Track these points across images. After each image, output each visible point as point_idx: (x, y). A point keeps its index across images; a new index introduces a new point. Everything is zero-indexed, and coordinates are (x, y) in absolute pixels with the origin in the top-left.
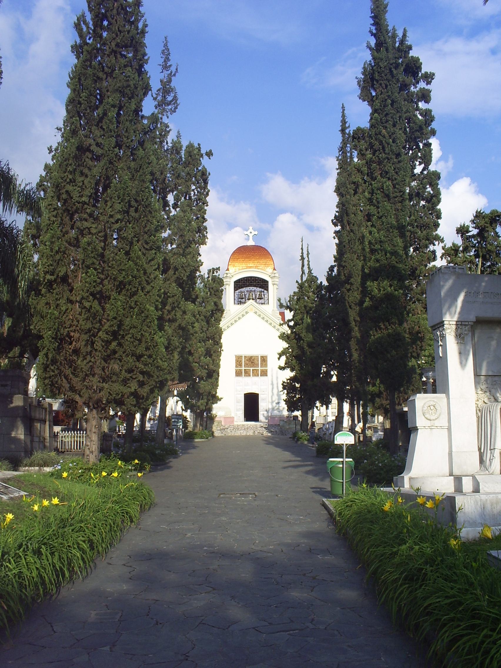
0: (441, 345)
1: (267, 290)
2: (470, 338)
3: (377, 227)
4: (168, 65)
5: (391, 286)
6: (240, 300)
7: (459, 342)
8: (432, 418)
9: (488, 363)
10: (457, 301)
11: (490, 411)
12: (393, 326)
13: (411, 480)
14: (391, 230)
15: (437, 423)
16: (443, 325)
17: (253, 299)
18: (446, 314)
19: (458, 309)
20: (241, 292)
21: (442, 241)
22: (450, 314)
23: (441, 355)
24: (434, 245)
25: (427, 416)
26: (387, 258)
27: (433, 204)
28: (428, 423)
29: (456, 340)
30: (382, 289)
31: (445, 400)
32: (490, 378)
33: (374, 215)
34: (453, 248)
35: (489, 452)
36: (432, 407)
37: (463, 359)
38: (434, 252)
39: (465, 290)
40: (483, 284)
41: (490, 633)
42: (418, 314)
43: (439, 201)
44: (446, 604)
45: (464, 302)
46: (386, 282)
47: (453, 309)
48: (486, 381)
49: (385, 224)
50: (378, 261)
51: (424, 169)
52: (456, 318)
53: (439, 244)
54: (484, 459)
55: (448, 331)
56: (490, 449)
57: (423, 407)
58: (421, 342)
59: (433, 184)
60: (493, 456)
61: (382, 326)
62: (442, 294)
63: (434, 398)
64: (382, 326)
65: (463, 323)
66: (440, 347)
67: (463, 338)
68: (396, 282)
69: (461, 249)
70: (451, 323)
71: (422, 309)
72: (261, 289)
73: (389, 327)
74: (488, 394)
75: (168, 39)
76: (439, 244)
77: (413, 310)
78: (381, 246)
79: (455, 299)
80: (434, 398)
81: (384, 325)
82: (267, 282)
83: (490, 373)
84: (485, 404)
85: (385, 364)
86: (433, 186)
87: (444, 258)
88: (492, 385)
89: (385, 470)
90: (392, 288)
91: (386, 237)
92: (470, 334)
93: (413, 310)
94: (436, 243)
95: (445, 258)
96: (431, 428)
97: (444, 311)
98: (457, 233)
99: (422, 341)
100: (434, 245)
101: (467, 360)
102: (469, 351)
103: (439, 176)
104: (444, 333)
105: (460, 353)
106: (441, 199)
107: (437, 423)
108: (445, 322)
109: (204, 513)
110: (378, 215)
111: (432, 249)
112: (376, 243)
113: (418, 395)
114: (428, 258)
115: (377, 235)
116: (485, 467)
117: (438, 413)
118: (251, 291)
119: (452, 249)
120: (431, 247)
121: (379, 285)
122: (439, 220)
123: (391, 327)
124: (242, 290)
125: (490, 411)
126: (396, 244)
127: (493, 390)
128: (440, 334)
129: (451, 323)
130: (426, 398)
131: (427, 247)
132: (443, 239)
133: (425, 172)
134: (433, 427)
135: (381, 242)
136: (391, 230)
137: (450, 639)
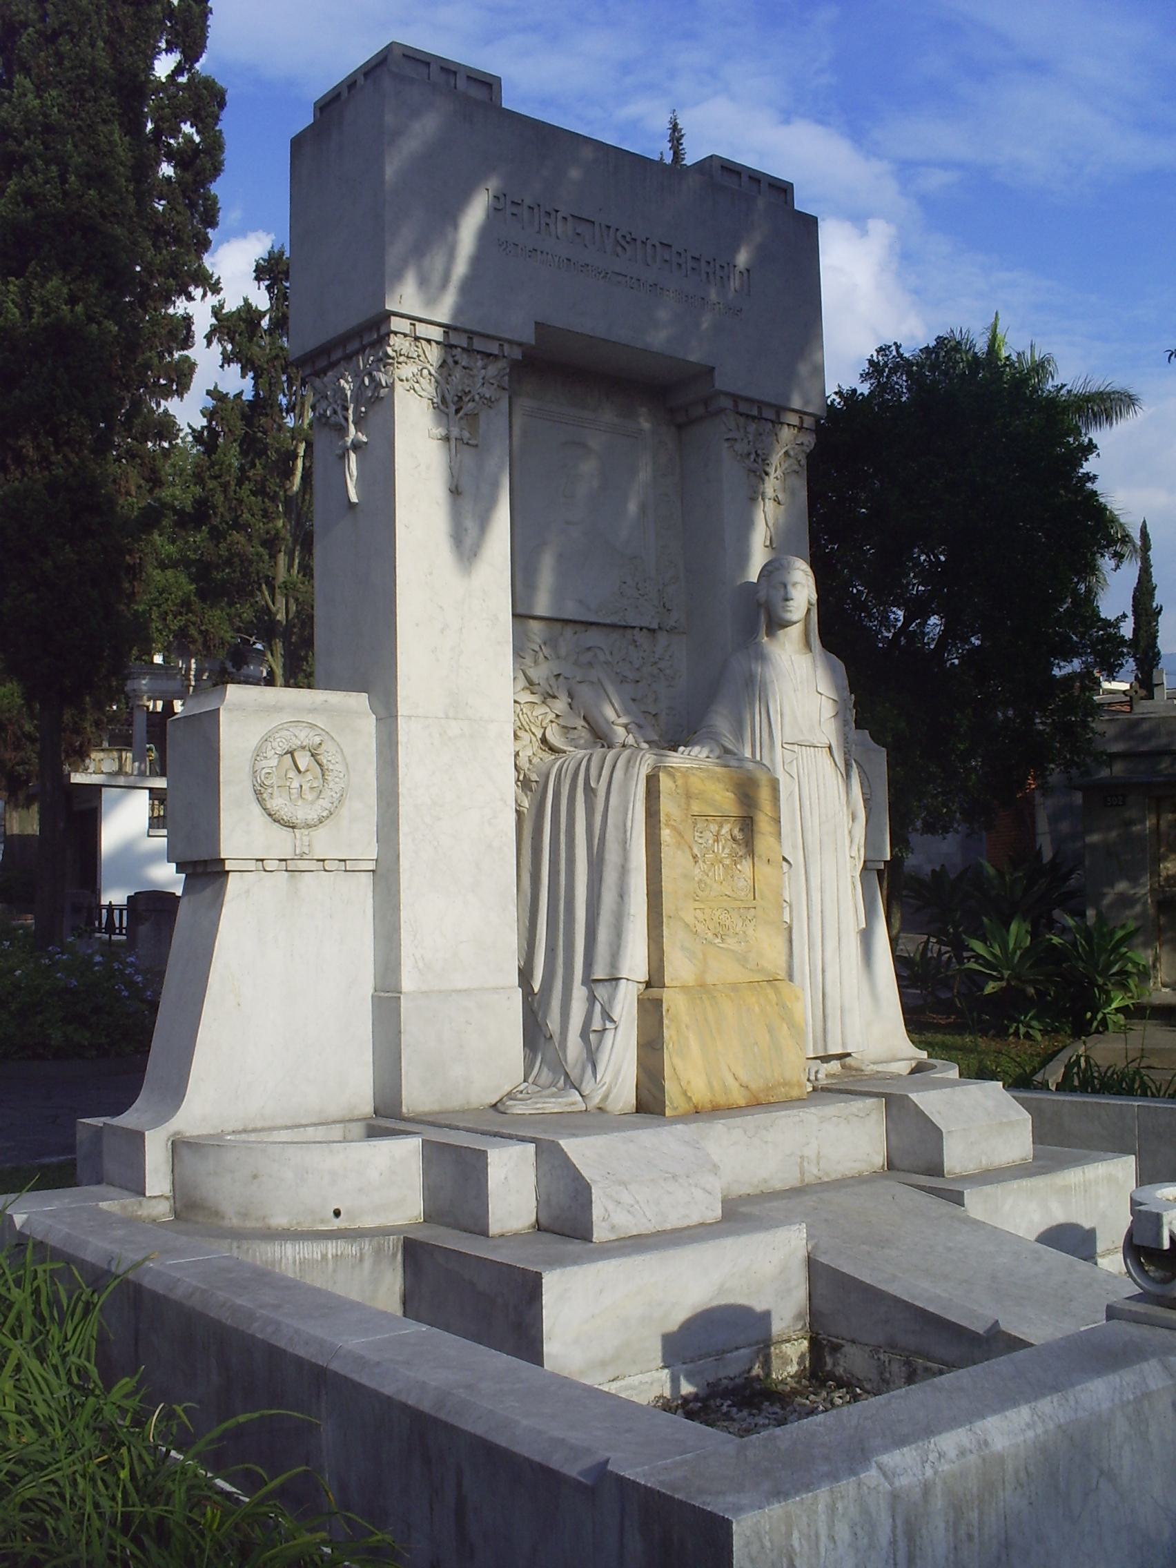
0: (357, 446)
2: (502, 423)
3: (35, 71)
5: (72, 300)
7: (455, 432)
8: (303, 812)
9: (560, 557)
10: (456, 226)
11: (590, 792)
12: (72, 456)
14: (91, 92)
15: (323, 843)
16: (383, 339)
18: (399, 276)
19: (461, 268)
21: (216, 289)
22: (423, 282)
23: (354, 498)
24: (190, 298)
25: (277, 803)
26: (65, 194)
27: (198, 174)
28: (279, 843)
29: (439, 423)
30: (38, 309)
31: (369, 724)
32: (569, 631)
33: (25, 25)
34: (243, 315)
35: (579, 993)
36: (304, 760)
37: (470, 524)
38: (187, 320)
39: (493, 184)
40: (574, 174)
42: (128, 494)
43: (217, 170)
44: (227, 1521)
45: (486, 235)
46: (53, 283)
47: (437, 261)
48: (551, 642)
49: (67, 63)
50: (28, 198)
51: (178, 70)
52: (443, 312)
53: (204, 295)
54: (553, 1024)
55: (407, 370)
56: (589, 981)
57: (258, 754)
58: (130, 582)
59: (203, 114)
60: (607, 1016)
61: (31, 452)
62: (390, 172)
63: (313, 710)
64: (31, 452)
65: (478, 344)
66: (353, 456)
67: (473, 418)
68: (93, 288)
69: (265, 323)
70: (422, 330)
71: (142, 482)
73: (54, 458)
74: (560, 705)
76: (204, 295)
77: (114, 481)
78: (46, 148)
79: (450, 216)
80: (313, 710)
81: (38, 447)
83: (571, 610)
84: (549, 757)
85: (31, 596)
86: (202, 121)
87: (215, 341)
88: (576, 663)
89: (13, 1007)
90: (79, 308)
91: (70, 116)
92: (504, 404)
93: (114, 481)
94: (197, 292)
95: (219, 341)
96: (290, 867)
97: (394, 252)
98: (258, 279)
99: (134, 579)
100: (190, 298)
101: (484, 521)
102: (495, 485)
103: (223, 98)
104: (383, 379)
105: (455, 491)
106: (222, 163)
107: (323, 843)
108: (396, 324)
110: (40, 26)
111: (181, 312)
112: (28, 133)
113: (234, 692)
114: (170, 332)
115: (32, 102)
116: (558, 1066)
117: (334, 785)
119: (241, 319)
120: (180, 307)
121: (25, 292)
122: (209, 230)
123: (65, 456)
125: (590, 792)
126: (106, 148)
127: (585, 692)
128: (359, 389)
129: (422, 330)
130: (277, 708)
131: (168, 301)
132: (218, 281)
133: (183, 79)
134: (302, 865)
135: (48, 129)
136: (91, 92)
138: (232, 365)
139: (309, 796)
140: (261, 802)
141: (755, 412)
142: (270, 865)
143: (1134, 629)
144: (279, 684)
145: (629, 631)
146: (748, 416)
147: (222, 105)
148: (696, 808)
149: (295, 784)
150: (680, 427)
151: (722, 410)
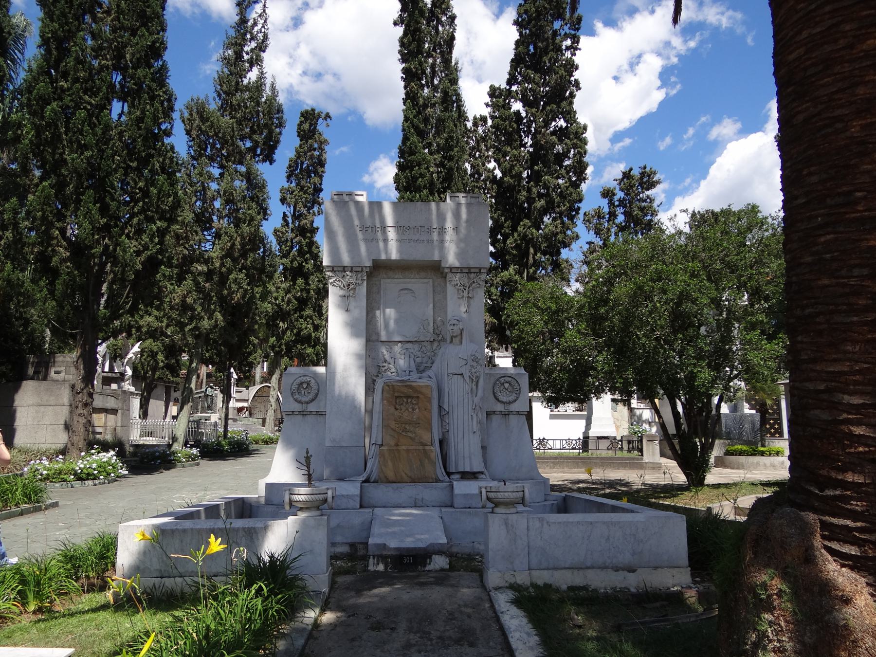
25: (297, 396)
148: (396, 394)
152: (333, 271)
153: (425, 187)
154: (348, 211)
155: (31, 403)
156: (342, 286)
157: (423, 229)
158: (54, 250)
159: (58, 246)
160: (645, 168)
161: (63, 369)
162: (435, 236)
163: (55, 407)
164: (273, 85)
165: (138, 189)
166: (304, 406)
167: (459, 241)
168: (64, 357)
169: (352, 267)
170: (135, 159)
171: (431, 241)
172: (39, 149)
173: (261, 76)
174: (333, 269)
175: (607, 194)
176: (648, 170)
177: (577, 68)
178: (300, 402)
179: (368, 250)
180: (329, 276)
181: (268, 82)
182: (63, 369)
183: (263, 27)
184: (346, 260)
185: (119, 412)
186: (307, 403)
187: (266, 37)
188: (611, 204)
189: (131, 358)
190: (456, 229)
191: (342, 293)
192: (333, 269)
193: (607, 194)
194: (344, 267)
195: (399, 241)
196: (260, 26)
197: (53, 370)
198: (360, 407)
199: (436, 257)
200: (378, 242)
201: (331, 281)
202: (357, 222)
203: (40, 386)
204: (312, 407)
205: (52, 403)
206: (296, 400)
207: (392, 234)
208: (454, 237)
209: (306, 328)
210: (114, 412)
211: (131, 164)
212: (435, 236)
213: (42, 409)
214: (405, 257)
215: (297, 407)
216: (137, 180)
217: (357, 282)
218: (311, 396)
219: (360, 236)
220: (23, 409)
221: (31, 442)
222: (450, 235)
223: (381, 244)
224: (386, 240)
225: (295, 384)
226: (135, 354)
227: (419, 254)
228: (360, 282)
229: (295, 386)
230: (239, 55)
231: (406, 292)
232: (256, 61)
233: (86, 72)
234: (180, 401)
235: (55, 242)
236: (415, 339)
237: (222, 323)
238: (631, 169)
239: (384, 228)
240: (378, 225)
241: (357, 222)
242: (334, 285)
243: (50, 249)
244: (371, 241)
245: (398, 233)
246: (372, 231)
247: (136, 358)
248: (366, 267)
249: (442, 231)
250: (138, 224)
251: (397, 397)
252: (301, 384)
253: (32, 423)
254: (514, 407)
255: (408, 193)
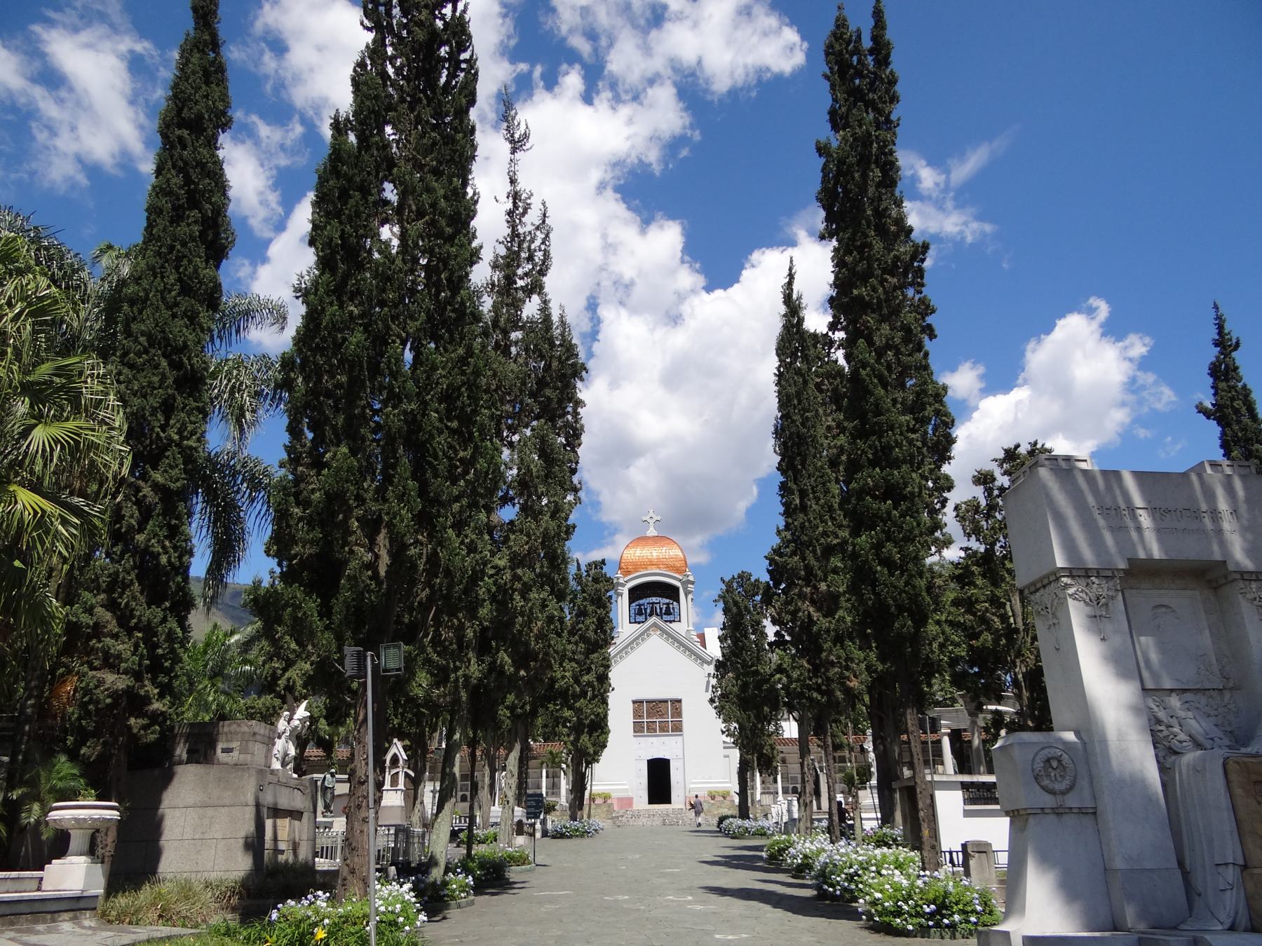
1: (678, 602)
4: (517, 136)
6: (639, 615)
13: (1088, 821)
17: (657, 614)
20: (640, 605)
25: (1046, 782)
36: (1055, 764)
41: (394, 771)
72: (667, 601)
75: (547, 205)
82: (677, 589)
109: (639, 910)
118: (653, 603)
124: (641, 602)
134: (1061, 810)
137: (20, 430)
138: (812, 331)
139: (1059, 779)
140: (1038, 783)
141: (1254, 578)
142: (1046, 811)
143: (1043, 675)
144: (1139, 374)
145: (1207, 692)
146: (1251, 580)
147: (833, 113)
148: (1254, 777)
149: (1053, 774)
150: (1215, 588)
151: (1235, 580)
152: (1071, 576)
153: (904, 462)
154: (1074, 483)
155: (191, 801)
156: (1088, 600)
157: (1188, 513)
158: (352, 552)
159: (357, 544)
160: (1036, 443)
161: (235, 745)
162: (1207, 522)
163: (233, 809)
164: (563, 322)
165: (459, 460)
166: (1059, 798)
167: (1244, 530)
168: (239, 725)
169: (1098, 570)
170: (457, 417)
171: (1203, 531)
172: (318, 400)
173: (545, 308)
174: (1071, 573)
175: (984, 479)
176: (1039, 446)
177: (933, 311)
178: (1052, 792)
179: (1117, 543)
180: (1066, 584)
181: (555, 318)
182: (235, 745)
183: (543, 243)
184: (1089, 558)
185: (305, 815)
186: (1063, 793)
187: (547, 255)
188: (989, 491)
189: (297, 727)
190: (1235, 512)
191: (1088, 609)
192: (1071, 573)
193: (984, 479)
194: (1087, 570)
195: (1159, 531)
196: (538, 242)
197: (220, 746)
198: (1158, 799)
199: (1217, 556)
200: (1128, 531)
201: (1071, 591)
202: (1091, 500)
203: (208, 774)
204: (1071, 801)
205: (227, 802)
206: (1044, 788)
207: (1145, 520)
208: (1235, 525)
209: (563, 677)
210: (296, 815)
211: (449, 424)
212: (1207, 522)
213: (210, 812)
214: (1174, 556)
215: (1048, 801)
216: (458, 447)
217: (1110, 594)
218: (1068, 782)
219: (1101, 522)
220: (177, 813)
221: (187, 868)
222: (1228, 525)
223: (1134, 535)
224: (1139, 529)
225: (1038, 760)
226: (302, 720)
227: (1190, 550)
228: (1114, 594)
229: (1039, 765)
230: (510, 280)
231: (1164, 610)
232: (536, 288)
233: (394, 292)
234: (469, 799)
235: (353, 538)
236: (1198, 686)
237: (512, 669)
238: (1018, 446)
239: (1132, 510)
240: (1123, 506)
241: (1091, 500)
242: (1075, 599)
243: (347, 549)
244: (1118, 529)
245: (1154, 519)
246: (1117, 514)
247: (303, 727)
248: (1118, 570)
249: (1215, 514)
250: (461, 512)
251: (1256, 783)
252: (1048, 761)
253: (190, 837)
254: (1071, 801)
255: (877, 469)
